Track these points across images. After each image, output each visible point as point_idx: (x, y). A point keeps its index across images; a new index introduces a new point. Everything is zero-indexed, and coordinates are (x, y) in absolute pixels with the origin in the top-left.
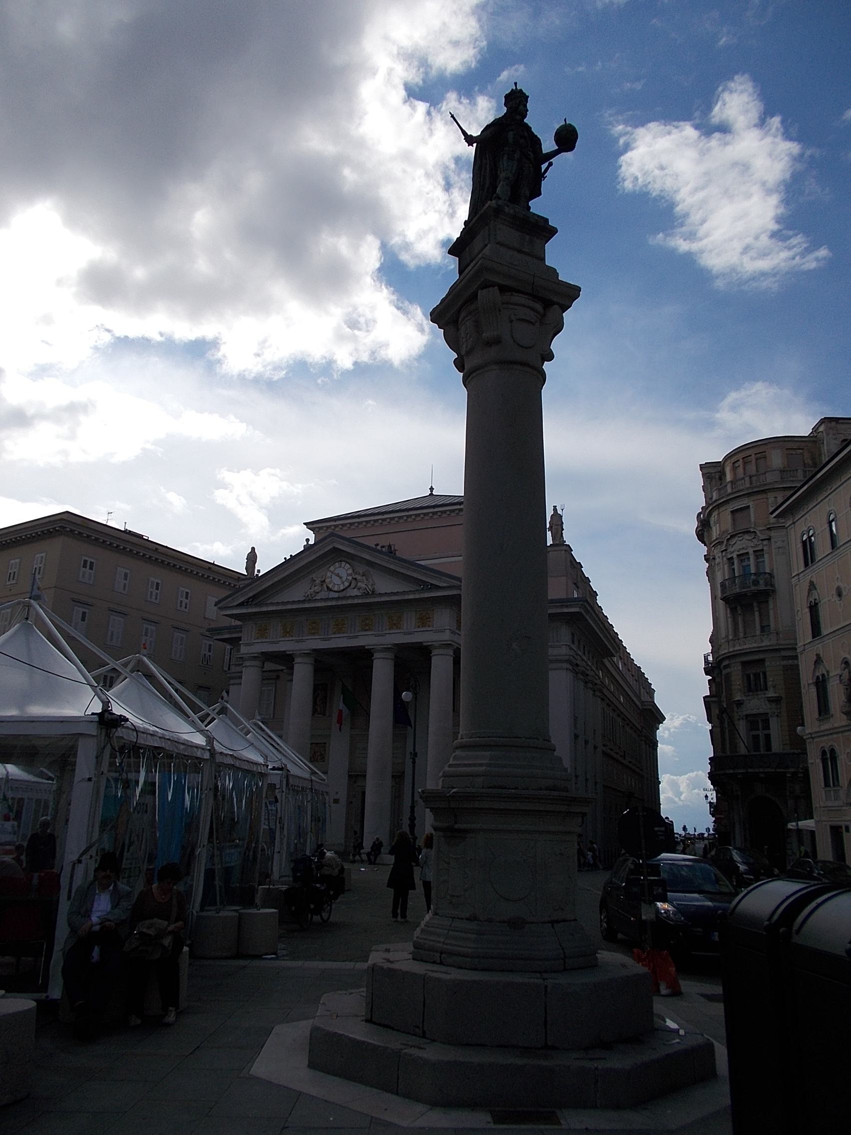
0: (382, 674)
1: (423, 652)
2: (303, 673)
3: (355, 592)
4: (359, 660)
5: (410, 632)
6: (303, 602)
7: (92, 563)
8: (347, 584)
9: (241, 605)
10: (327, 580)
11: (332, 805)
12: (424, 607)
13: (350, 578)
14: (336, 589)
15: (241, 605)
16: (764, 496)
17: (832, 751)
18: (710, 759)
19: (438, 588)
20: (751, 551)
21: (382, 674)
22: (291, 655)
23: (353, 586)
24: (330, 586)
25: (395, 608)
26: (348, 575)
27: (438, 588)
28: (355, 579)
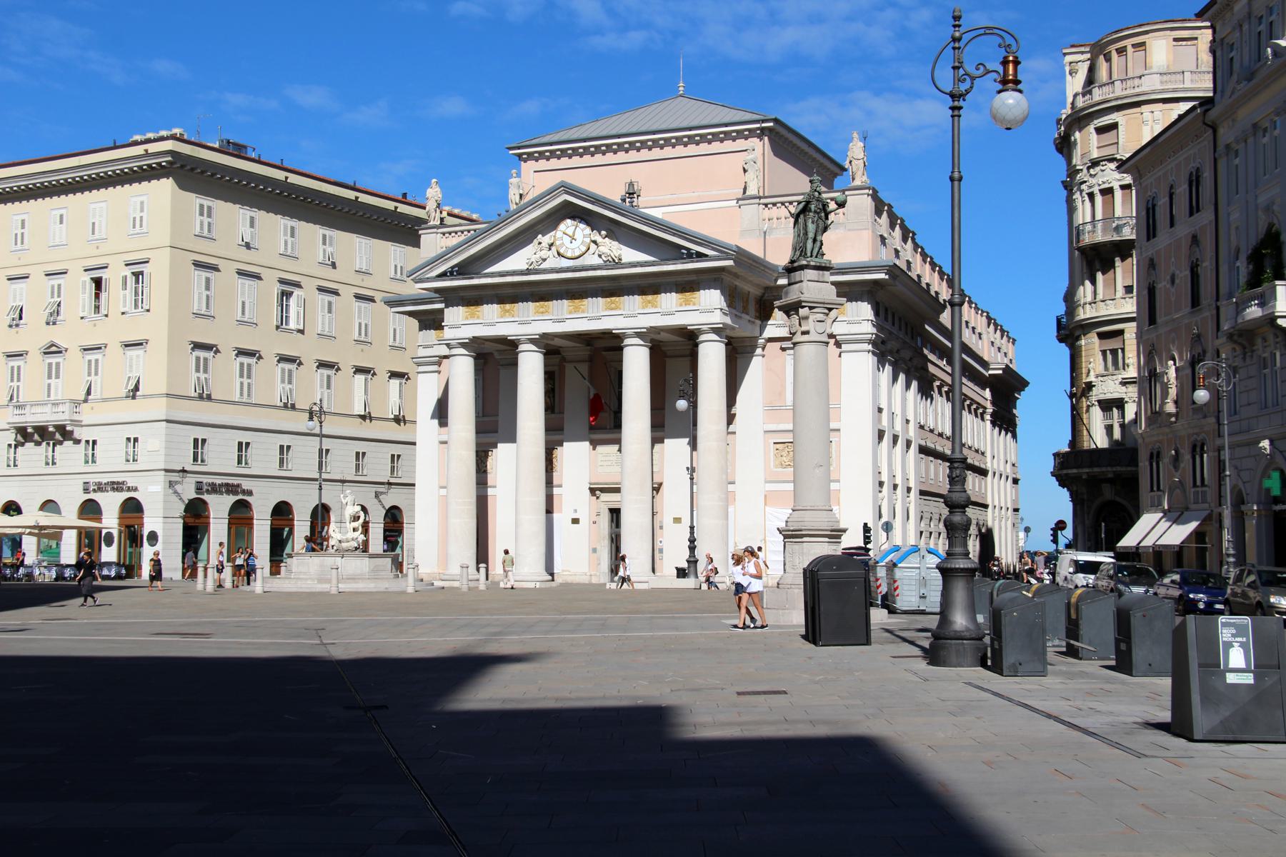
0: (636, 367)
1: (689, 338)
2: (531, 368)
3: (596, 261)
4: (602, 351)
5: (669, 311)
6: (528, 272)
7: (209, 208)
8: (584, 249)
9: (443, 276)
10: (558, 243)
11: (58, 213)
12: (687, 284)
13: (588, 240)
14: (569, 255)
15: (443, 276)
16: (1137, 110)
17: (1158, 453)
18: (1056, 455)
19: (700, 256)
20: (1116, 185)
21: (636, 367)
22: (512, 341)
23: (591, 251)
24: (562, 251)
25: (648, 286)
26: (585, 236)
27: (700, 256)
28: (595, 242)
